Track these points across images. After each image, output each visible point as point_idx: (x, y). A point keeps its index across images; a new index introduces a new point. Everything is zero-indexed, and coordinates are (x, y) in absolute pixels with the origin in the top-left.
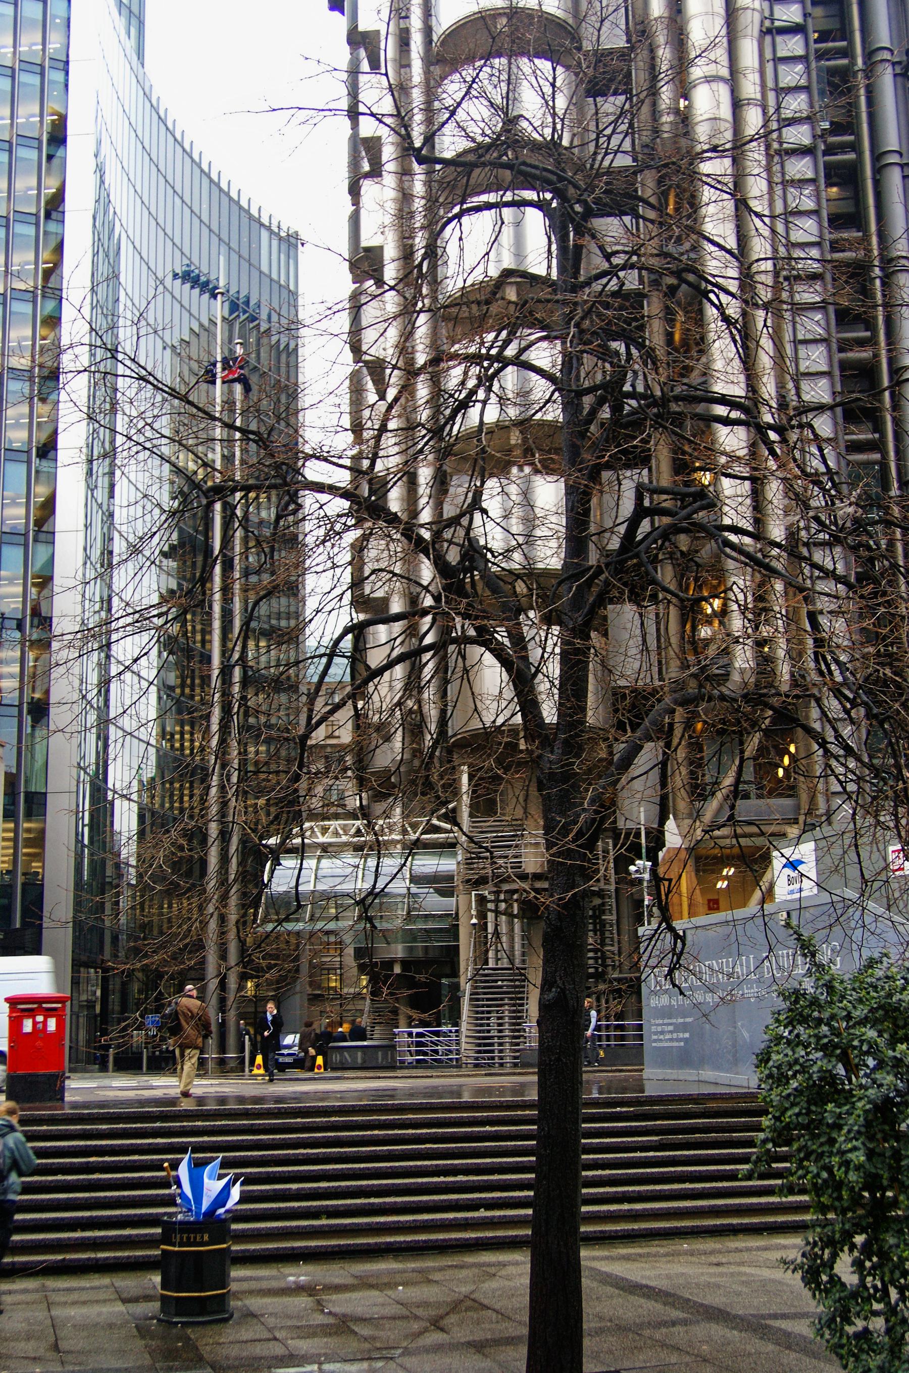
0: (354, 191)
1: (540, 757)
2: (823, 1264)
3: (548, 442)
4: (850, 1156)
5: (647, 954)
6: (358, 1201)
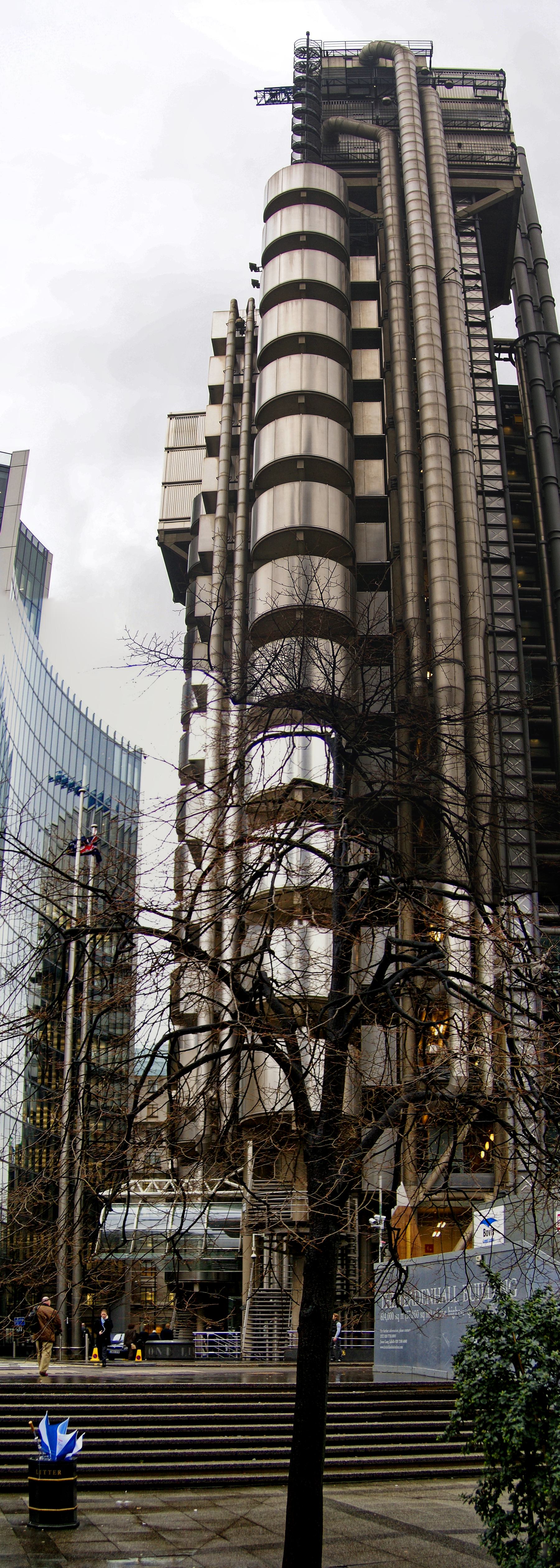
0: (186, 721)
1: (307, 1136)
2: (491, 1498)
3: (321, 903)
4: (515, 1426)
5: (379, 1283)
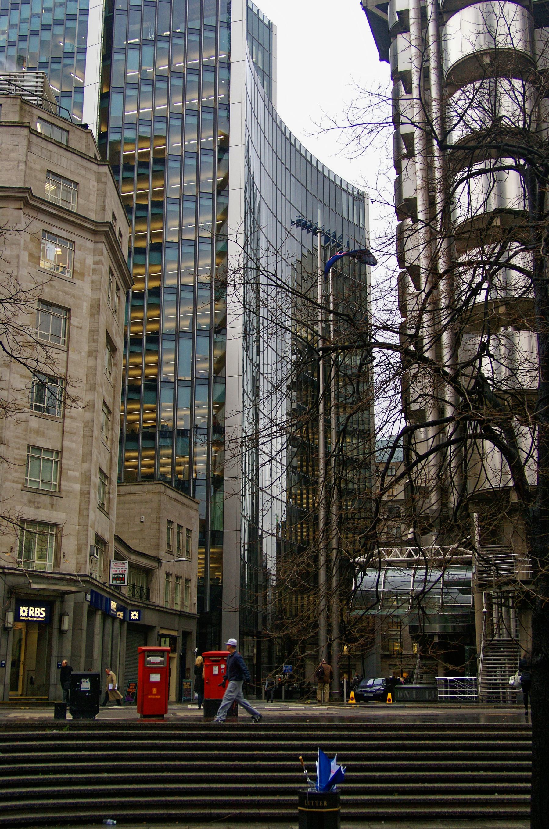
0: (398, 166)
6: (417, 785)
